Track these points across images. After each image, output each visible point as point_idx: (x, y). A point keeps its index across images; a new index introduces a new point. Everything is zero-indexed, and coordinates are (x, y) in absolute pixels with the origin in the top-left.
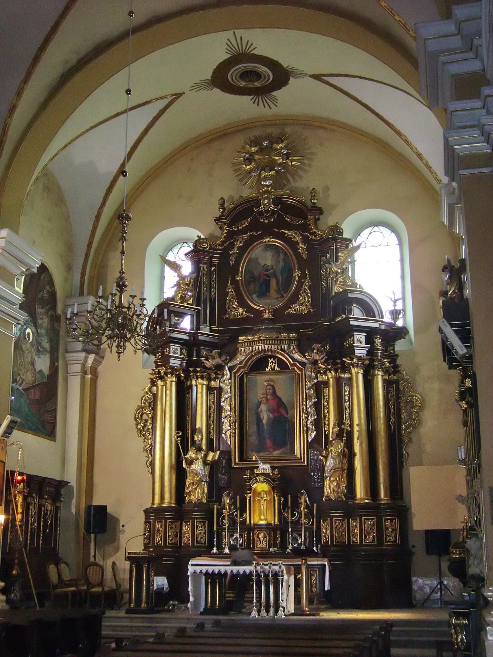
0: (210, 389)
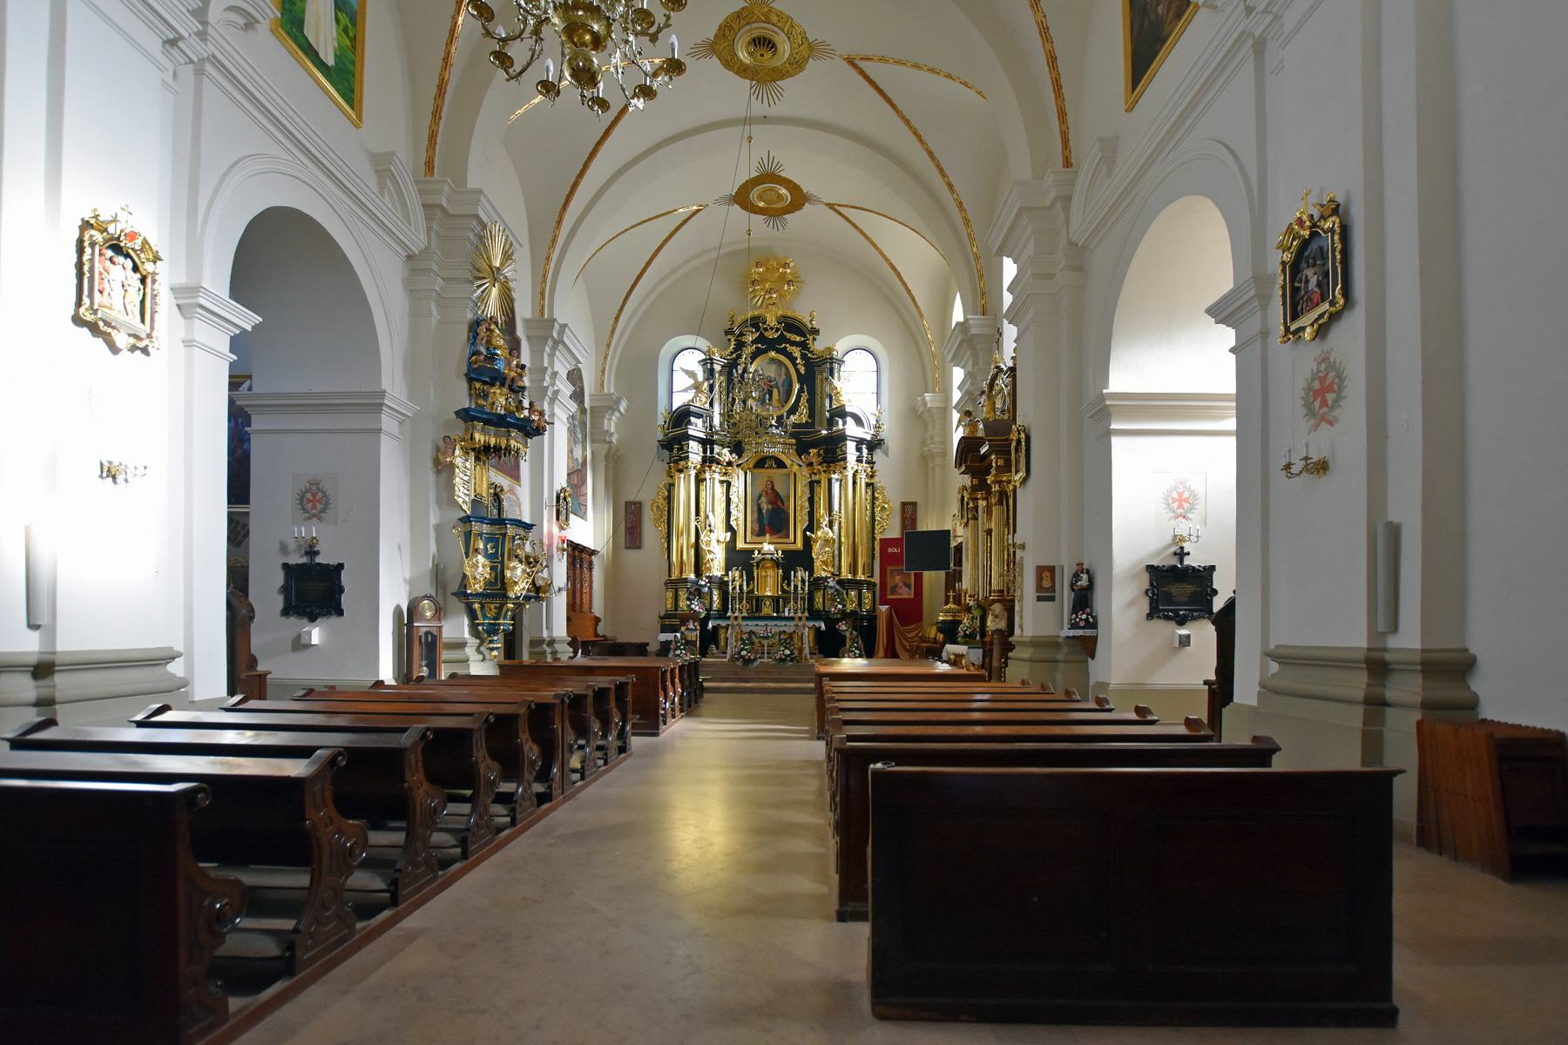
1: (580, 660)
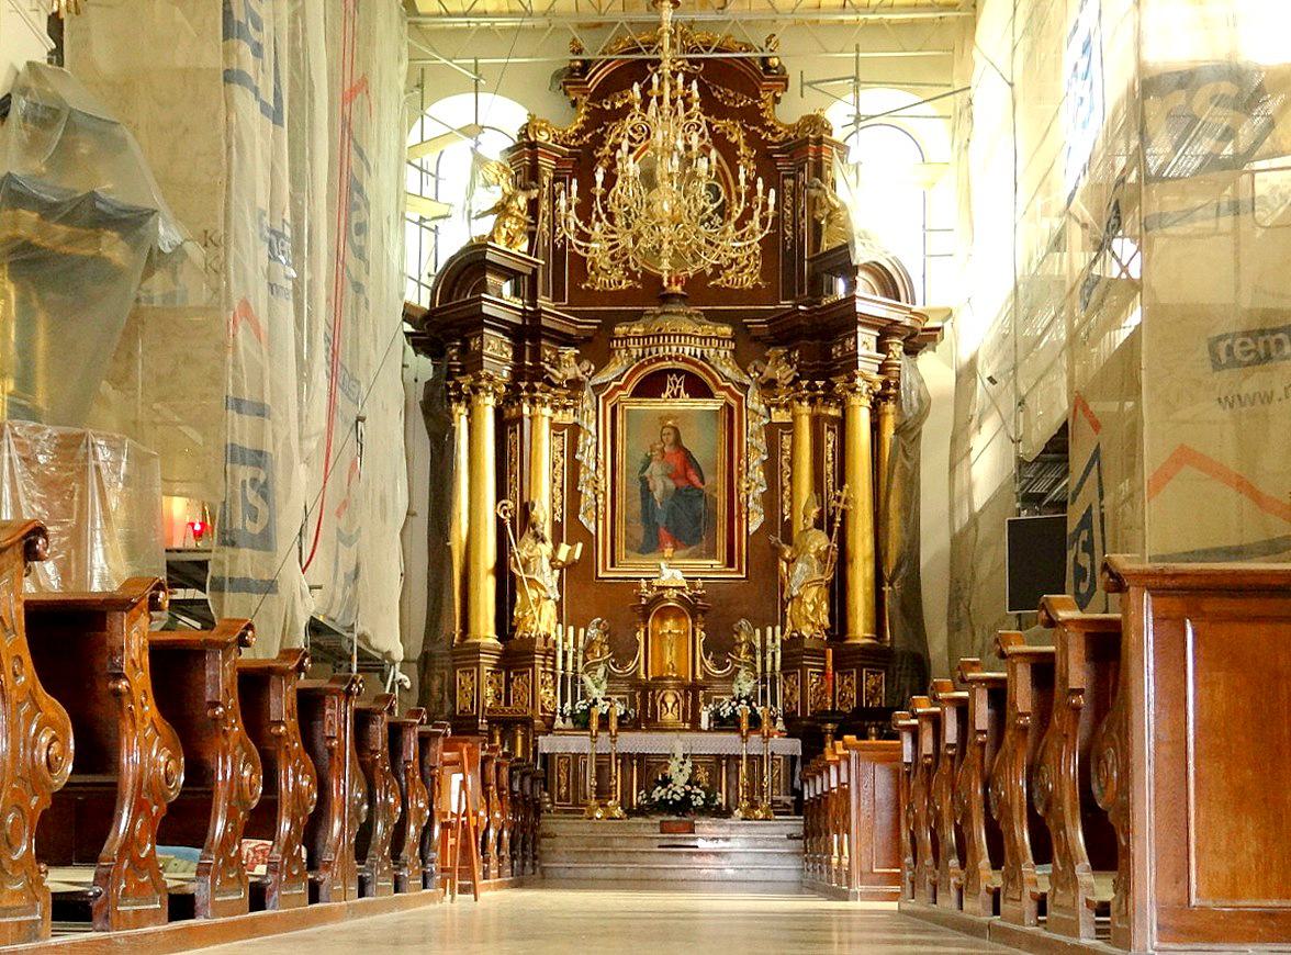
0: (556, 427)
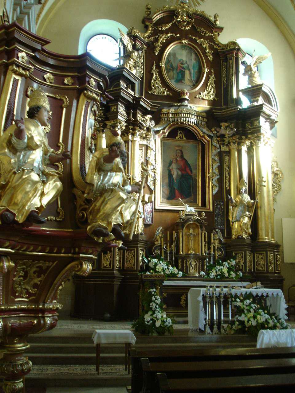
0: (141, 145)
1: (127, 370)
